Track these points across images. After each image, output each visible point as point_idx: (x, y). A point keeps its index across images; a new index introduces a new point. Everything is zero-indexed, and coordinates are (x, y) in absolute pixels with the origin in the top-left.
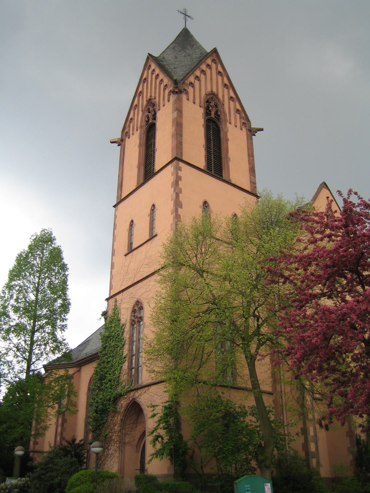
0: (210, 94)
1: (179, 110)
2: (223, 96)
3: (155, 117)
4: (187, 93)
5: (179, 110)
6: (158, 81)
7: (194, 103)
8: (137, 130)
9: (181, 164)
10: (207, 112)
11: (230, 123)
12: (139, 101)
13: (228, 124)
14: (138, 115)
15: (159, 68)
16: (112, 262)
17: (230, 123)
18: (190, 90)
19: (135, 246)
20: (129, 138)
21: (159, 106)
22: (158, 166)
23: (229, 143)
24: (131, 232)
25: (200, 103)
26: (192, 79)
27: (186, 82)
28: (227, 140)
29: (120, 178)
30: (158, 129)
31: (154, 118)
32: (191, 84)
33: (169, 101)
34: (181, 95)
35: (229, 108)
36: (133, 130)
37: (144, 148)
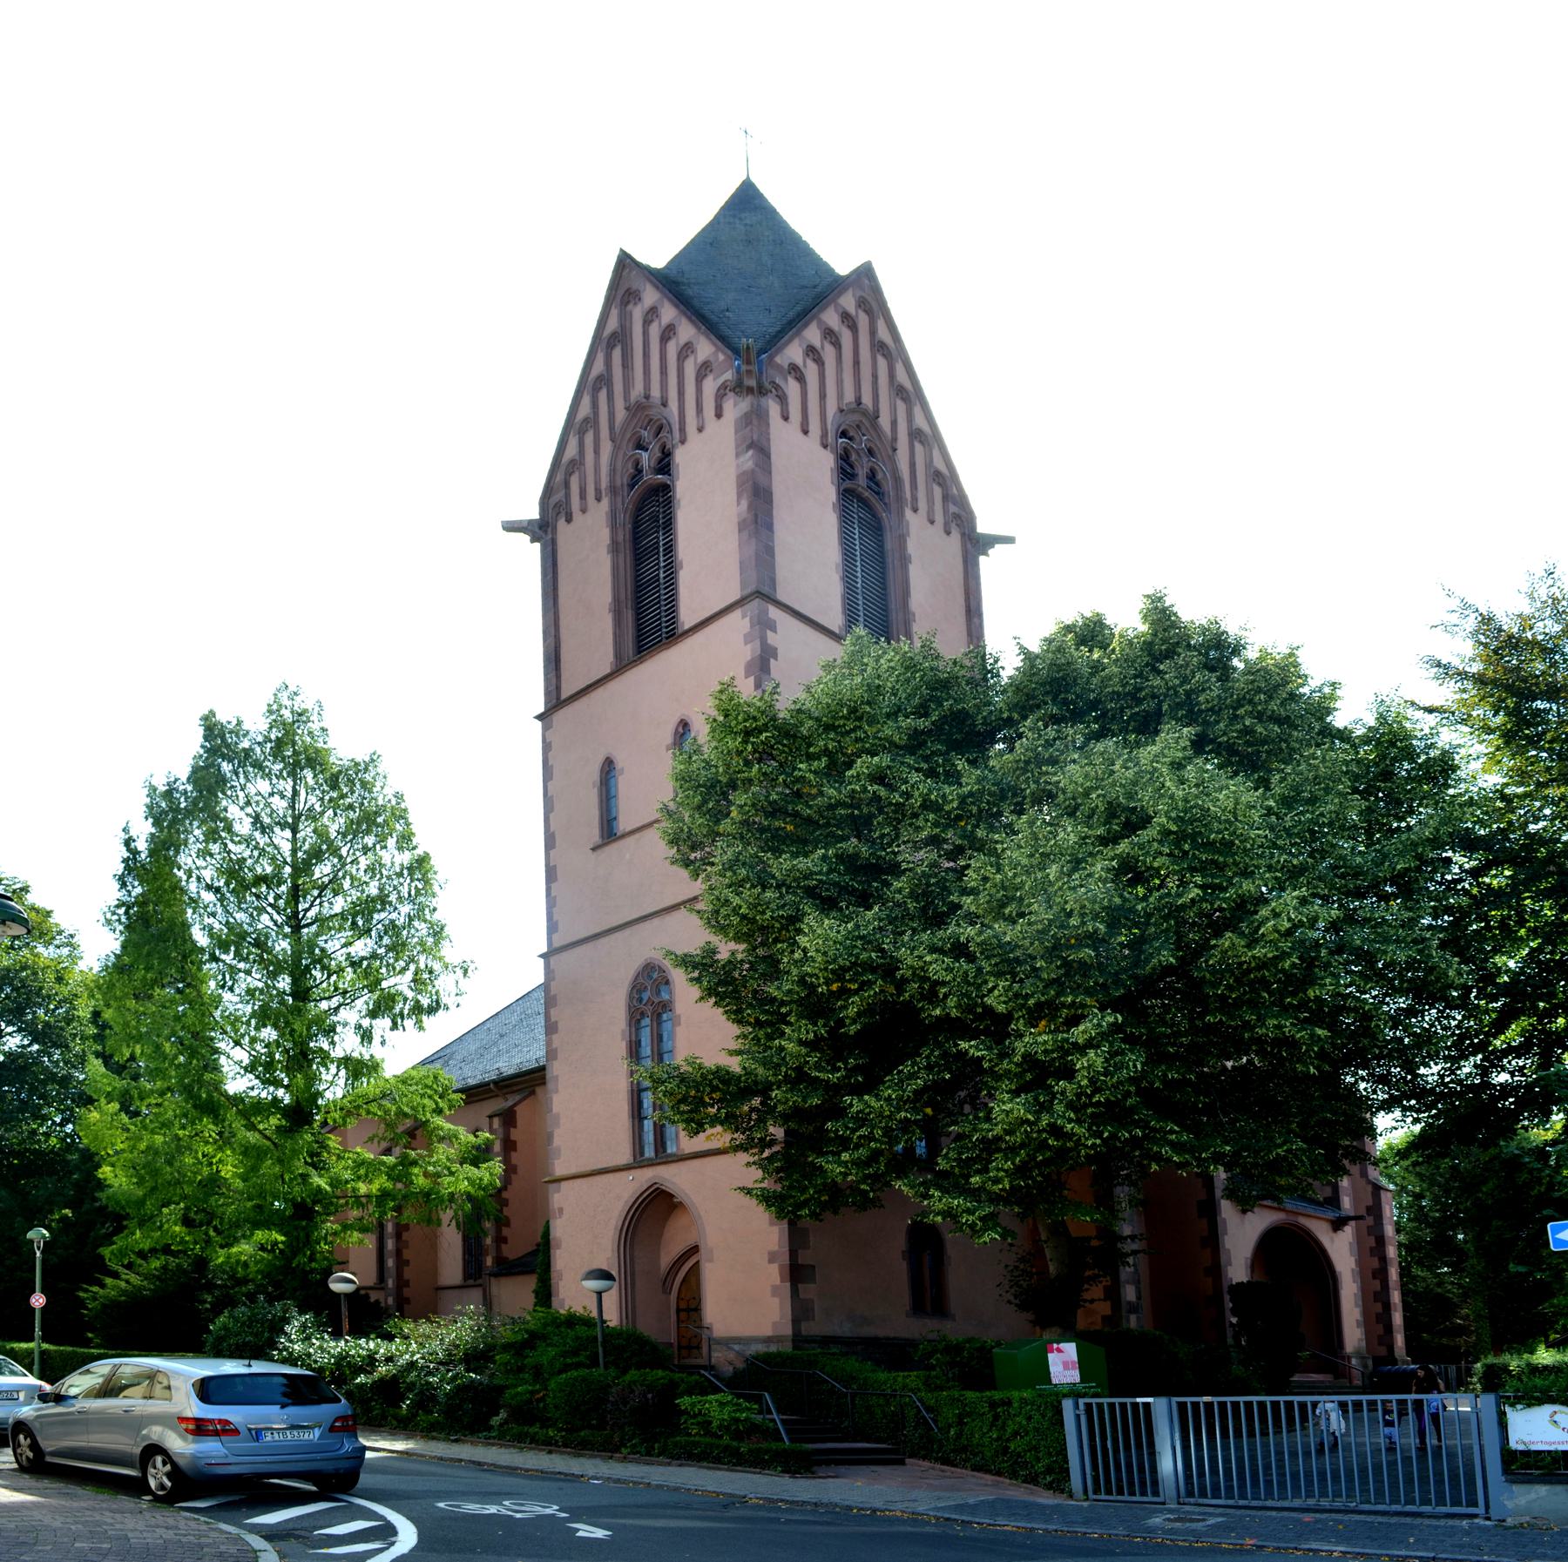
0: (853, 411)
1: (757, 445)
2: (894, 423)
3: (669, 464)
4: (782, 399)
5: (757, 445)
6: (672, 349)
7: (806, 432)
8: (598, 499)
9: (774, 613)
10: (845, 469)
11: (915, 510)
12: (595, 405)
13: (908, 513)
14: (597, 452)
15: (676, 306)
16: (547, 865)
17: (915, 510)
18: (792, 388)
19: (624, 823)
20: (569, 520)
21: (682, 430)
22: (691, 606)
23: (912, 568)
24: (608, 791)
25: (824, 435)
26: (793, 352)
27: (778, 359)
28: (905, 560)
29: (552, 640)
30: (682, 503)
31: (665, 464)
32: (795, 371)
33: (719, 415)
34: (763, 400)
35: (913, 465)
36: (583, 496)
37: (626, 558)
